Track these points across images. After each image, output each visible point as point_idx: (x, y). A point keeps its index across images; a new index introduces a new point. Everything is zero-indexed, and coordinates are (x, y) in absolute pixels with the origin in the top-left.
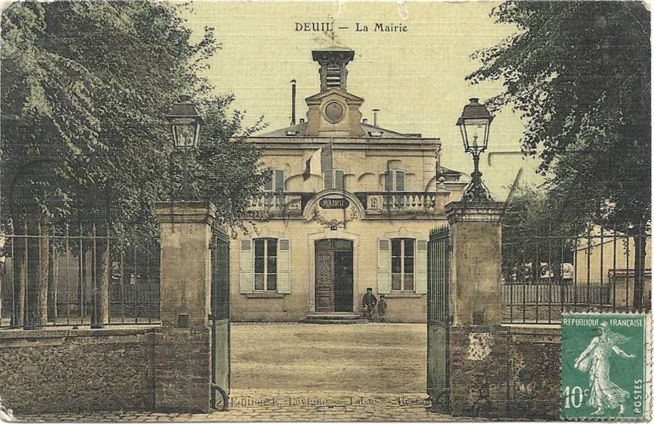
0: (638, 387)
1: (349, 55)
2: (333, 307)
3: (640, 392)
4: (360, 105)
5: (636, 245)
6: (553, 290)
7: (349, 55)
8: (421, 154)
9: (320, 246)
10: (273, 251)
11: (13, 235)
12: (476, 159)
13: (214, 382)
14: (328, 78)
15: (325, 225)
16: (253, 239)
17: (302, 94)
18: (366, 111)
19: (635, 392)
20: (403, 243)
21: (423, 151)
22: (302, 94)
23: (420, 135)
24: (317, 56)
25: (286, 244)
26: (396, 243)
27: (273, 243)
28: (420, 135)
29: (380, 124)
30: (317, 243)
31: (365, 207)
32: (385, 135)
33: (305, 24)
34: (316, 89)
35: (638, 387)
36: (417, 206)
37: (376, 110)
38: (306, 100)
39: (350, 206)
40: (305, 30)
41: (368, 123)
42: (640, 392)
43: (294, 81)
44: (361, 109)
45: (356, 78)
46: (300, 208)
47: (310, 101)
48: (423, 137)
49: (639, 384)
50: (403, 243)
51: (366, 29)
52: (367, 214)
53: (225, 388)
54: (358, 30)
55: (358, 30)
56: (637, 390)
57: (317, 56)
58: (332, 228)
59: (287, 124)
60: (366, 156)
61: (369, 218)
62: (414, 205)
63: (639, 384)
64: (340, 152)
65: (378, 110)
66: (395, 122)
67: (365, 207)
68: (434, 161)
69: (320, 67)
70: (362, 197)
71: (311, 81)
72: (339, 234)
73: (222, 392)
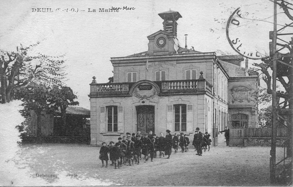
6: (234, 131)
8: (205, 61)
10: (116, 113)
14: (167, 27)
15: (140, 99)
16: (174, 105)
25: (191, 108)
26: (109, 108)
27: (184, 107)
33: (38, 9)
37: (17, 49)
38: (147, 37)
39: (153, 88)
40: (38, 11)
46: (128, 90)
51: (94, 11)
54: (89, 11)
55: (89, 11)
60: (177, 63)
65: (17, 47)
72: (147, 103)
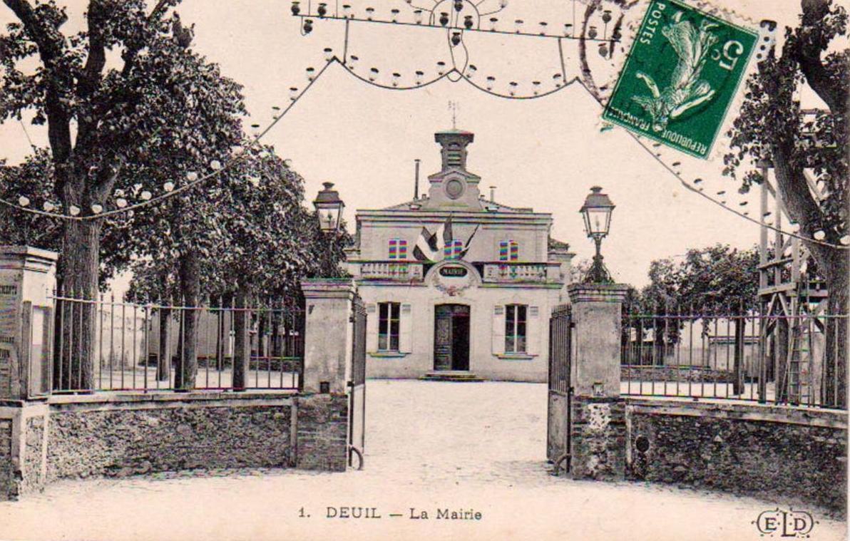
0: (648, 34)
1: (469, 137)
2: (450, 366)
3: (648, 28)
4: (478, 182)
5: (286, 344)
7: (469, 137)
8: (534, 227)
9: (440, 311)
10: (522, 316)
11: (184, 307)
12: (598, 244)
13: (351, 443)
17: (424, 174)
18: (483, 187)
19: (654, 30)
20: (390, 307)
21: (536, 225)
22: (424, 174)
23: (531, 210)
24: (439, 137)
25: (535, 309)
26: (510, 308)
27: (522, 309)
28: (531, 210)
29: (496, 200)
30: (437, 307)
31: (482, 276)
32: (501, 210)
34: (438, 169)
35: (648, 34)
36: (530, 276)
41: (485, 198)
42: (648, 28)
43: (418, 160)
44: (480, 186)
45: (475, 159)
47: (432, 179)
48: (534, 212)
49: (646, 37)
50: (390, 307)
52: (483, 282)
53: (360, 449)
56: (650, 32)
57: (439, 137)
58: (451, 295)
59: (410, 198)
61: (485, 284)
62: (527, 275)
63: (646, 37)
64: (459, 225)
66: (509, 197)
67: (482, 276)
68: (545, 234)
69: (442, 148)
70: (479, 266)
71: (433, 160)
73: (358, 453)
